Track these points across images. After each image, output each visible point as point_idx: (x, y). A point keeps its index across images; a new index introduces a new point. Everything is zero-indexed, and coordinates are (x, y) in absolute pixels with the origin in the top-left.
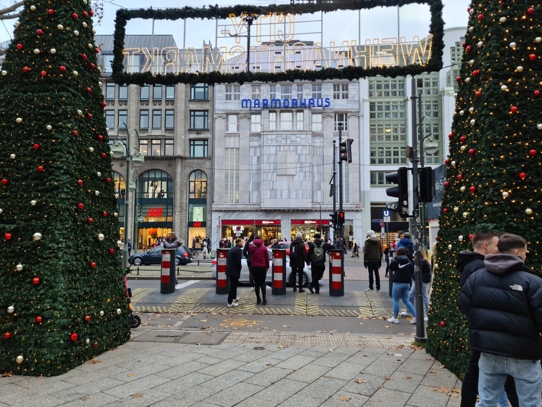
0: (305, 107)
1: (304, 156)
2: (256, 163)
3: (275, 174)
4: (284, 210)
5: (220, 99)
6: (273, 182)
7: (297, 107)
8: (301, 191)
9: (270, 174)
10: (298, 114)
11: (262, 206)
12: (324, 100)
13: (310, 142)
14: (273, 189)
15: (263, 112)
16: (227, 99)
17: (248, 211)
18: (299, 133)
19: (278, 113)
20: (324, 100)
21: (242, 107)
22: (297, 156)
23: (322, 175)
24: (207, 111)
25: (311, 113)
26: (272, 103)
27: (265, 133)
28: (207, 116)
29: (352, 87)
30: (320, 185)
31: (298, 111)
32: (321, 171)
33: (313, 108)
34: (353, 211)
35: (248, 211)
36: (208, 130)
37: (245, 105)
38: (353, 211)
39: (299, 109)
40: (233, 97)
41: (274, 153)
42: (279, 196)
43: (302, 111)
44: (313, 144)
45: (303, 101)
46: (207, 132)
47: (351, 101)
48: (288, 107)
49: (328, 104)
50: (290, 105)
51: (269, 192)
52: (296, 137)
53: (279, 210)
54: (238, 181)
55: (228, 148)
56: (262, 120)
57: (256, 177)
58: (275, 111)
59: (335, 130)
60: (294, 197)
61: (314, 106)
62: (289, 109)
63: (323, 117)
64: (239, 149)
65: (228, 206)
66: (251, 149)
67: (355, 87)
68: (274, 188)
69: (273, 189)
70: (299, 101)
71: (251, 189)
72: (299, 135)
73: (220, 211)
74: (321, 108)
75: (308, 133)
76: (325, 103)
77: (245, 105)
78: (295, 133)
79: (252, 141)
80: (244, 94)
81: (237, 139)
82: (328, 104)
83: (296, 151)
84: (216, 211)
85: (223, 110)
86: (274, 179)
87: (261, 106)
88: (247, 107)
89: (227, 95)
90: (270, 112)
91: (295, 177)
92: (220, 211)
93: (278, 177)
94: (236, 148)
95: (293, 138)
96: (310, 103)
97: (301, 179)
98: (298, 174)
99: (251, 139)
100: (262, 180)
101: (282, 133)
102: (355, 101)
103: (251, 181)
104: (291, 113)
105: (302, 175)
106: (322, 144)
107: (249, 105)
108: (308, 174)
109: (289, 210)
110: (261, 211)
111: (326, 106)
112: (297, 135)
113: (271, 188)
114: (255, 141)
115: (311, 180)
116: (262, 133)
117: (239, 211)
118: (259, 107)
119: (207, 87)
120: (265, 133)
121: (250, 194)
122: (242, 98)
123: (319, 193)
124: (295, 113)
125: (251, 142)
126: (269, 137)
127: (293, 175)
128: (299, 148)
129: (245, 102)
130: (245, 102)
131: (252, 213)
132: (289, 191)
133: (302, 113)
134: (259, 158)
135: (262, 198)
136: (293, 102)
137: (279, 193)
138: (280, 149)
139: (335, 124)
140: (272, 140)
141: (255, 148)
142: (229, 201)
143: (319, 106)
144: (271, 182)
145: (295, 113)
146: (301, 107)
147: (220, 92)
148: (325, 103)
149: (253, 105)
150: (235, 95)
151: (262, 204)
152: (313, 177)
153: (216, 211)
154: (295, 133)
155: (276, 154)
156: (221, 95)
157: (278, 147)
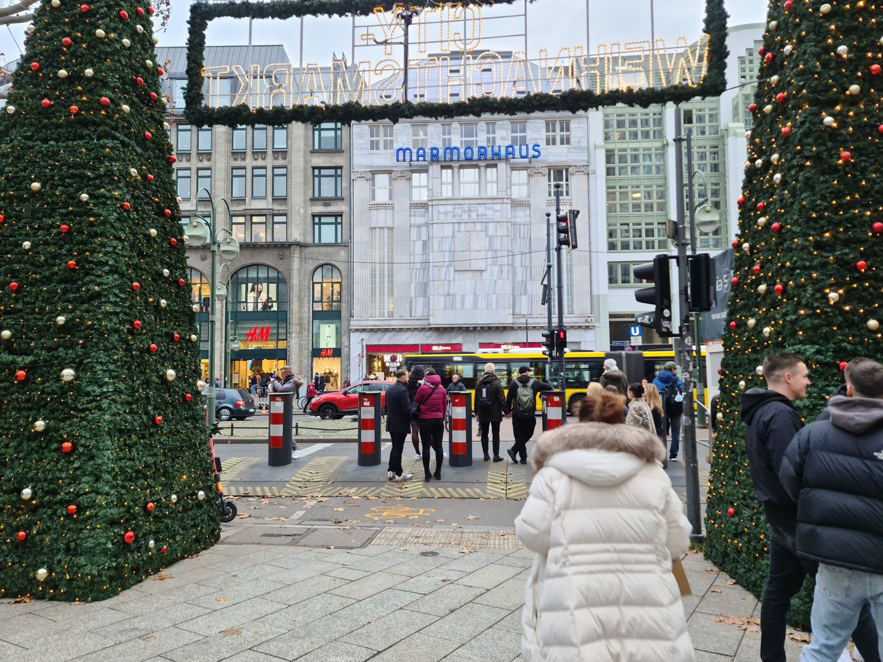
0: (500, 159)
1: (499, 239)
2: (421, 252)
3: (452, 269)
4: (467, 328)
5: (361, 148)
6: (449, 281)
7: (486, 159)
8: (494, 297)
9: (444, 270)
10: (489, 170)
11: (431, 322)
12: (530, 147)
13: (509, 216)
14: (449, 294)
15: (431, 169)
16: (372, 148)
17: (408, 329)
18: (489, 201)
19: (456, 170)
20: (530, 147)
21: (398, 161)
22: (488, 239)
23: (529, 269)
24: (341, 168)
25: (509, 169)
26: (445, 153)
27: (434, 203)
28: (341, 176)
29: (577, 125)
30: (525, 286)
31: (488, 166)
32: (528, 263)
33: (512, 160)
34: (580, 327)
35: (408, 329)
36: (342, 199)
37: (401, 158)
38: (580, 327)
39: (489, 162)
40: (381, 145)
41: (450, 234)
42: (458, 306)
43: (495, 166)
44: (513, 220)
45: (496, 149)
46: (340, 203)
47: (575, 148)
48: (471, 159)
49: (536, 153)
50: (476, 157)
51: (442, 299)
52: (486, 208)
53: (460, 328)
54: (391, 282)
55: (375, 228)
56: (430, 181)
57: (421, 275)
58: (450, 167)
59: (550, 195)
60: (484, 307)
61: (514, 158)
62: (474, 163)
63: (529, 176)
64: (391, 229)
65: (377, 323)
66: (412, 229)
67: (581, 125)
68: (451, 292)
69: (449, 294)
70: (489, 149)
71: (413, 295)
72: (491, 206)
73: (364, 330)
74: (526, 160)
75: (505, 201)
76: (532, 153)
77: (401, 158)
78: (484, 201)
79: (414, 216)
80: (399, 140)
81: (389, 212)
82: (536, 153)
83: (486, 231)
84: (357, 330)
85: (366, 167)
86: (451, 278)
87: (428, 158)
88: (404, 160)
89: (372, 142)
90: (443, 167)
91: (484, 273)
92: (364, 330)
93: (457, 274)
94: (389, 228)
95: (481, 210)
96: (508, 153)
97: (495, 278)
98: (489, 268)
99: (412, 213)
100: (431, 279)
101: (462, 202)
102: (582, 148)
103: (414, 281)
104: (477, 170)
105: (496, 269)
106: (528, 219)
107: (408, 158)
108: (505, 268)
109: (475, 328)
110: (431, 329)
111: (534, 157)
112: (487, 206)
113: (446, 292)
114: (420, 216)
115: (511, 278)
116: (430, 203)
117: (393, 330)
118: (424, 160)
119: (340, 129)
120: (434, 203)
121: (411, 302)
122: (397, 146)
123: (524, 299)
124: (483, 169)
125: (412, 218)
126: (442, 209)
127: (481, 271)
128: (491, 226)
129: (401, 152)
130: (401, 152)
131: (416, 333)
132: (476, 297)
133: (494, 170)
134: (425, 243)
135: (431, 308)
136: (479, 151)
137: (458, 299)
138: (459, 228)
139: (550, 185)
140: (446, 213)
141: (419, 226)
142: (377, 315)
143: (522, 157)
144: (446, 283)
145: (483, 169)
146: (493, 159)
147: (361, 136)
148: (532, 153)
149: (414, 158)
150: (386, 141)
151: (431, 318)
152: (514, 274)
153: (357, 330)
154: (484, 201)
155: (453, 236)
156: (363, 142)
157: (456, 225)
